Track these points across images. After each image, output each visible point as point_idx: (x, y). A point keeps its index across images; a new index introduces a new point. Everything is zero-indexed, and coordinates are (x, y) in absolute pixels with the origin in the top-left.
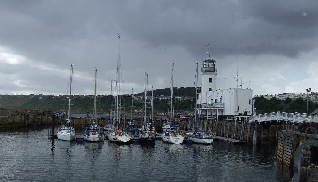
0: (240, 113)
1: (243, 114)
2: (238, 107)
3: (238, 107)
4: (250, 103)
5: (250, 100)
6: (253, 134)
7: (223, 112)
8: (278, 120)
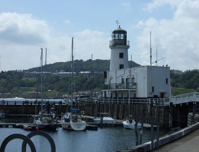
0: (156, 94)
1: (159, 95)
2: (153, 88)
3: (153, 88)
4: (167, 83)
5: (167, 79)
6: (168, 119)
7: (135, 94)
8: (195, 102)
